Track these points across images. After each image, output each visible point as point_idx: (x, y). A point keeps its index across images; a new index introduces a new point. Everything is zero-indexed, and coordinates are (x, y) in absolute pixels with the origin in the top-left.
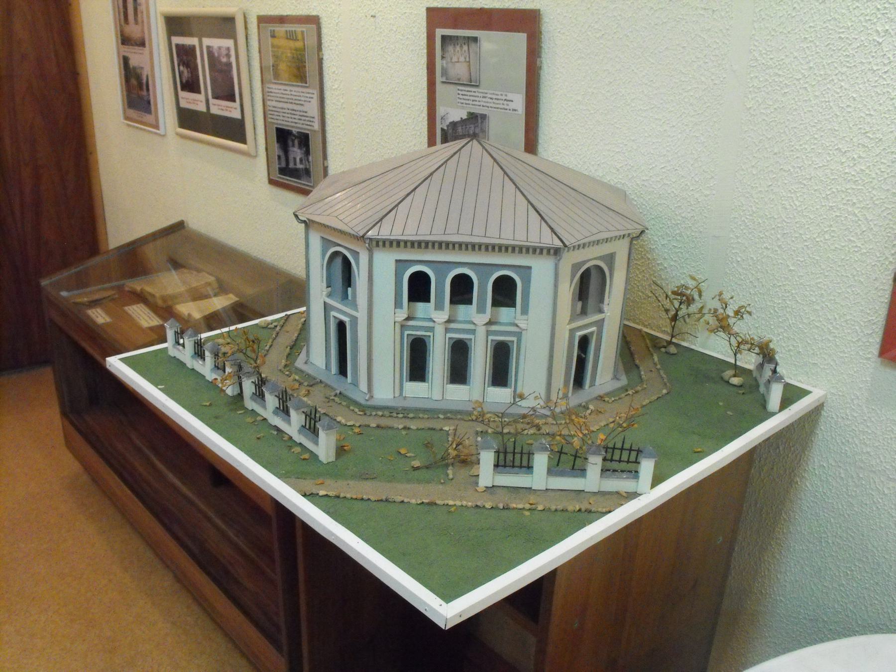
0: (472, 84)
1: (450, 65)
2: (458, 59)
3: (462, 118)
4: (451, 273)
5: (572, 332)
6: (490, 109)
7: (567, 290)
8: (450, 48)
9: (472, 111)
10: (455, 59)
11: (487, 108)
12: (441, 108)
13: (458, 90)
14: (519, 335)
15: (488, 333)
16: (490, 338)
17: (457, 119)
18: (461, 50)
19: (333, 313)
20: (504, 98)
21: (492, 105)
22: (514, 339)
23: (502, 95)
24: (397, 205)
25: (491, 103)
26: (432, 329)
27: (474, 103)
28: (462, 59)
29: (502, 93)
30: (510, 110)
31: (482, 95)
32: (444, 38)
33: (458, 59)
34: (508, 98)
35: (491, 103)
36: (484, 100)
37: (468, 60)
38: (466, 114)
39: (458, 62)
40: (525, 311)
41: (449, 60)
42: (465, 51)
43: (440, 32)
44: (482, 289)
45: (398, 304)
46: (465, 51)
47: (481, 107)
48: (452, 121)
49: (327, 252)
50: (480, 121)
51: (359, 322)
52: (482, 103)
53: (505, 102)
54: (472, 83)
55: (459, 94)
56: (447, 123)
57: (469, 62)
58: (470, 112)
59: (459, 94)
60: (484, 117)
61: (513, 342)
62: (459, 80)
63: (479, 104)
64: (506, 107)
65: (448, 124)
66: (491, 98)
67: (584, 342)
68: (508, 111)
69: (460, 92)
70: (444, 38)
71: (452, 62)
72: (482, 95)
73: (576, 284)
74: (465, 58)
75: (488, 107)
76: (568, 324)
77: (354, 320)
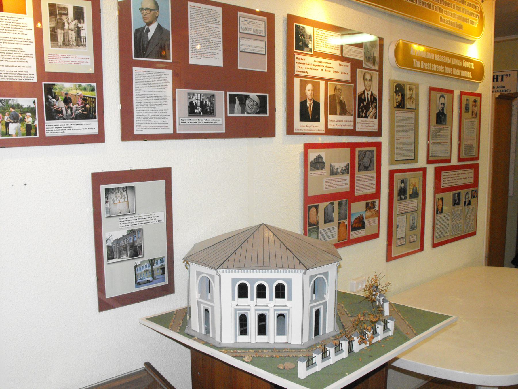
0: (353, 113)
1: (113, 206)
2: (119, 201)
3: (123, 235)
4: (276, 282)
5: (311, 308)
6: (143, 224)
7: (309, 289)
8: (113, 196)
9: (131, 229)
10: (116, 202)
11: (142, 225)
12: (106, 233)
13: (120, 219)
14: (288, 310)
15: (275, 310)
16: (276, 312)
17: (120, 236)
18: (122, 195)
19: (202, 305)
20: (153, 216)
21: (145, 222)
22: (287, 312)
23: (151, 215)
24: (242, 244)
25: (144, 221)
26: (249, 310)
27: (132, 224)
28: (122, 200)
29: (151, 214)
30: (157, 221)
31: (137, 218)
32: (107, 190)
33: (119, 201)
34: (155, 216)
35: (144, 221)
36: (139, 220)
37: (126, 200)
38: (127, 232)
39: (119, 202)
40: (290, 299)
41: (112, 203)
42: (124, 196)
43: (103, 188)
44: (270, 291)
45: (233, 299)
46: (124, 196)
47: (138, 225)
48: (116, 239)
49: (199, 277)
50: (137, 233)
51: (215, 308)
52: (137, 223)
53: (154, 218)
54: (130, 212)
55: (120, 221)
56: (112, 241)
57: (128, 201)
58: (129, 230)
59: (120, 221)
60: (139, 230)
61: (286, 313)
62: (120, 213)
63: (136, 223)
64: (154, 221)
65: (113, 241)
66: (144, 218)
67: (317, 313)
68: (156, 222)
69: (121, 220)
70: (107, 190)
71: (115, 204)
72: (137, 218)
73: (312, 286)
74: (125, 200)
75: (142, 224)
76: (310, 304)
77: (213, 307)
